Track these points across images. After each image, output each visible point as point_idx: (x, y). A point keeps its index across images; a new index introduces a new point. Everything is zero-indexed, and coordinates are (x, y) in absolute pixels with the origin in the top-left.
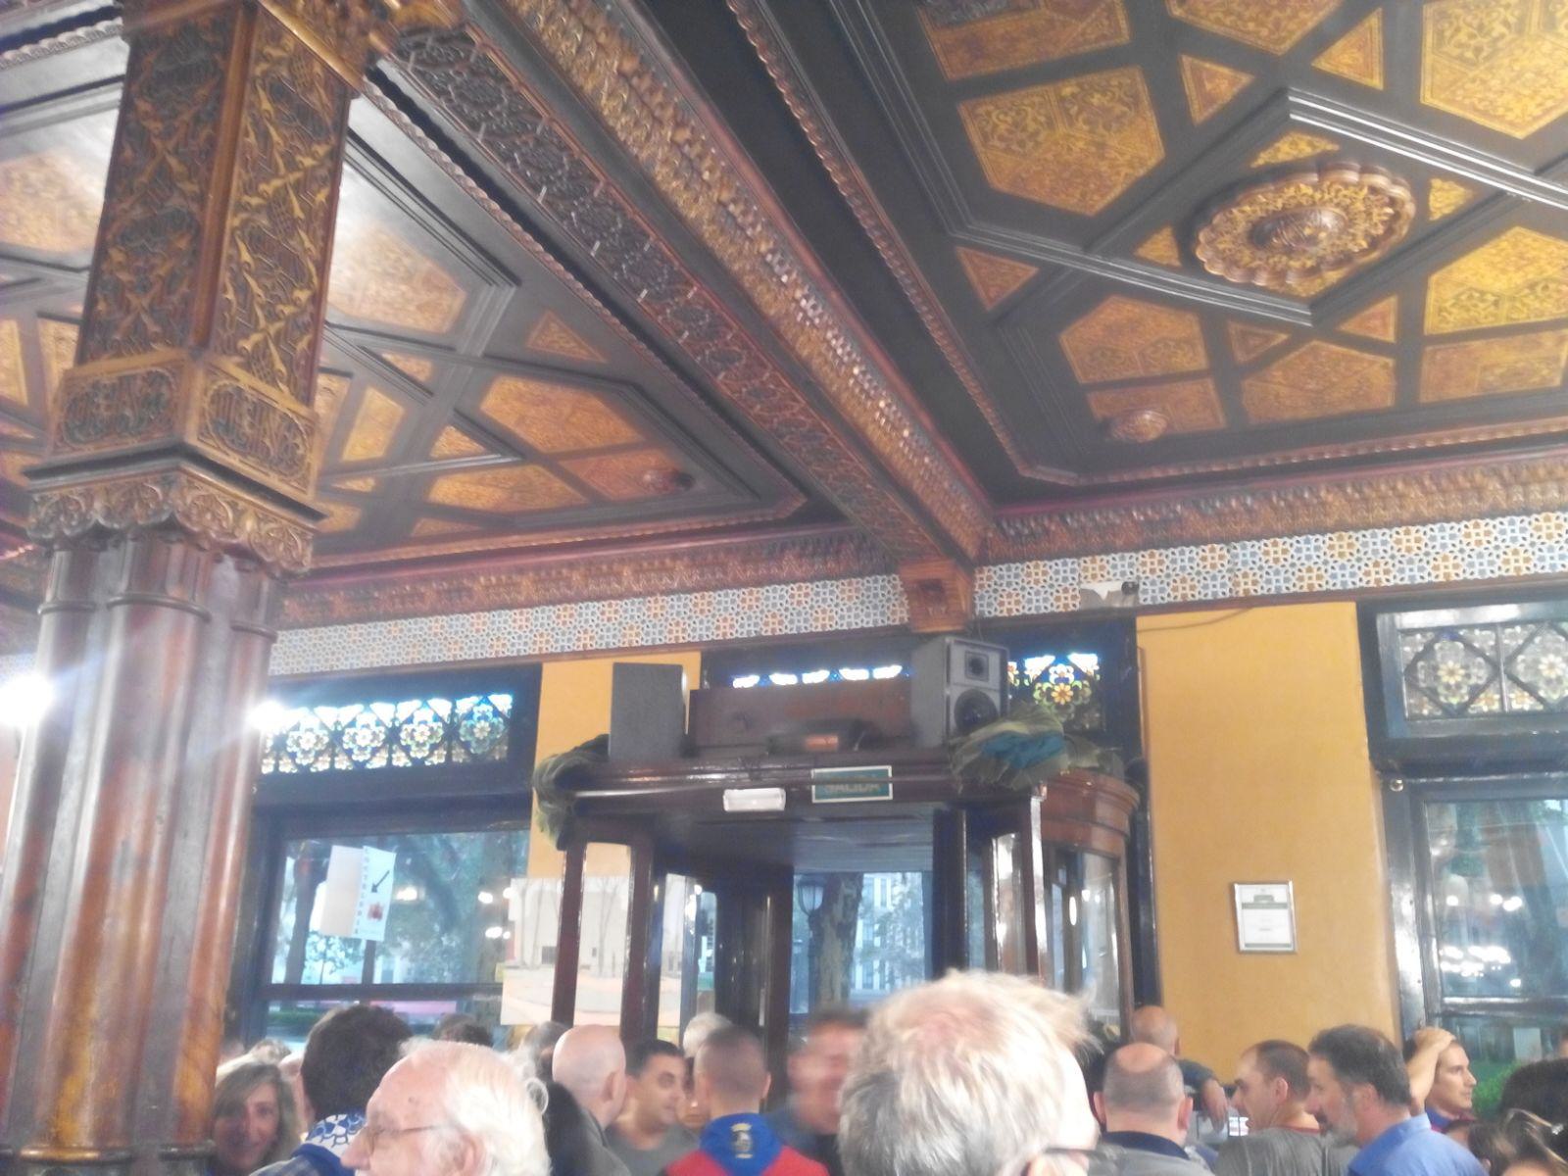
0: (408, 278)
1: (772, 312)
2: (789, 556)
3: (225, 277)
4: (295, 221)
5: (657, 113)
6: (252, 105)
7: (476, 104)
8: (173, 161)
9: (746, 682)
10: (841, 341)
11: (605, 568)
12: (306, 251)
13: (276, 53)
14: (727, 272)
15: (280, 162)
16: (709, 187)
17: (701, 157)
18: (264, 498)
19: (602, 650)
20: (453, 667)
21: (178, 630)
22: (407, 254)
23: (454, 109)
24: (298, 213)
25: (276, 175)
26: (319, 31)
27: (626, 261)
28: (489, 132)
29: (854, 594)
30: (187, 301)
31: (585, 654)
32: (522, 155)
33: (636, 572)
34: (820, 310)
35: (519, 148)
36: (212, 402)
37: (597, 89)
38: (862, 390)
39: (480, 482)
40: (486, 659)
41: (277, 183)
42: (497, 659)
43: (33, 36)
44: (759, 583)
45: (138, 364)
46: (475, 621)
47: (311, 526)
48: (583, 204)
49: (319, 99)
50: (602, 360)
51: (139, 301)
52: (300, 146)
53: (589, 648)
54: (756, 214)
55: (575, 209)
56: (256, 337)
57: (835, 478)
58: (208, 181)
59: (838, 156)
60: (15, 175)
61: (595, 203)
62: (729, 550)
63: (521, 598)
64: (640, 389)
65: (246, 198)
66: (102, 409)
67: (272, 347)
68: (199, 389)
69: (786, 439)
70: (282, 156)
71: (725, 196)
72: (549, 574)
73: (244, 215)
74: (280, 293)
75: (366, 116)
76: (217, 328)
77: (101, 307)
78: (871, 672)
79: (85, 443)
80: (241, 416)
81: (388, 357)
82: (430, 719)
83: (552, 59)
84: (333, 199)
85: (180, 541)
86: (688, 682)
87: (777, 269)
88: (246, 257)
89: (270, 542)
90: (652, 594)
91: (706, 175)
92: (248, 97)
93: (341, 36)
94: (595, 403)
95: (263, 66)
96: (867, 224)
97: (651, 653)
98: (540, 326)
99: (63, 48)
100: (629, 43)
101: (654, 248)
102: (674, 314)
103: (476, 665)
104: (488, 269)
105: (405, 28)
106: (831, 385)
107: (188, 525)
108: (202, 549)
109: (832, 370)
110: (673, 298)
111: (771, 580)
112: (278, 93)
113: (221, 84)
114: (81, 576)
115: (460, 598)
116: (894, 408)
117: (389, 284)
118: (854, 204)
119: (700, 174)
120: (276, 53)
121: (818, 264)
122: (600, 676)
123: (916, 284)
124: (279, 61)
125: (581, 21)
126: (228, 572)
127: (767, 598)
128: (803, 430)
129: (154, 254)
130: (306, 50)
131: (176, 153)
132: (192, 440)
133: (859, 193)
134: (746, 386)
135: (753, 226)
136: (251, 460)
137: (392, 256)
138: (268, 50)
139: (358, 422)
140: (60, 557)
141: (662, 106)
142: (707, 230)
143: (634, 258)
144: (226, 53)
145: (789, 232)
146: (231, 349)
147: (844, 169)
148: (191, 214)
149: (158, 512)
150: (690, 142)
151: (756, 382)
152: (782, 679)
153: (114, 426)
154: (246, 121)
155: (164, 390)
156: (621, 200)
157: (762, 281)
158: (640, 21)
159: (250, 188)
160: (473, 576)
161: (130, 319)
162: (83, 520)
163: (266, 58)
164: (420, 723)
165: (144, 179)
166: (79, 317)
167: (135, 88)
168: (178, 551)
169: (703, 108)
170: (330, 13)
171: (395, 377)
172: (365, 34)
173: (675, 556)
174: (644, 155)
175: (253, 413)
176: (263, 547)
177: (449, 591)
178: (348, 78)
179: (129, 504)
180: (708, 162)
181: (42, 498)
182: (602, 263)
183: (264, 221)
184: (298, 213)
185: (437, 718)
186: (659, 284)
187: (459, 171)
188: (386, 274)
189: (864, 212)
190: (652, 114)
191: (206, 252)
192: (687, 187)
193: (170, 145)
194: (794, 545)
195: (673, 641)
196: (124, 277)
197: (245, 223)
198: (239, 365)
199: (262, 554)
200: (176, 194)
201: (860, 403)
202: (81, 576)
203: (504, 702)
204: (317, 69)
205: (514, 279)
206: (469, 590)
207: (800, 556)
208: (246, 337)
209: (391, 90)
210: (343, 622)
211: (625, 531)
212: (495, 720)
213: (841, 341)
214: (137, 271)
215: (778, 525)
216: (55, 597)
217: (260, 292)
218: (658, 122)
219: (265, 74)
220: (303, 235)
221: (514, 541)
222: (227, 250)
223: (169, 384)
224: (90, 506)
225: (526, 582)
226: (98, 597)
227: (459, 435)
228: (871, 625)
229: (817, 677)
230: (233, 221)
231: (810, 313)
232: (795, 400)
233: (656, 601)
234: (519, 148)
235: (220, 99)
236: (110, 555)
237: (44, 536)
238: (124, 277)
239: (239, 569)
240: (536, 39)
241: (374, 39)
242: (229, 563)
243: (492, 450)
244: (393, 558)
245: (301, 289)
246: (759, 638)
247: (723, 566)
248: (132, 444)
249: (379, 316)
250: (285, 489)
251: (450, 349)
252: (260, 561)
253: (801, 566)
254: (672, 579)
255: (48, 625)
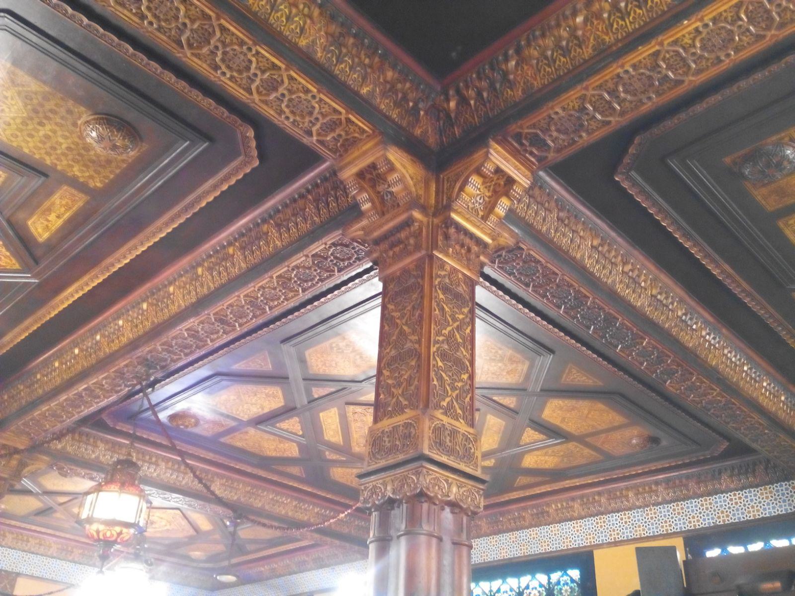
0: (502, 360)
1: (691, 345)
2: (724, 476)
3: (432, 374)
4: (458, 344)
5: (613, 260)
6: (436, 297)
7: (527, 276)
8: (405, 328)
9: (713, 553)
10: (733, 354)
11: (618, 493)
12: (464, 356)
13: (443, 273)
14: (662, 329)
15: (450, 319)
16: (646, 289)
17: (639, 276)
18: (459, 476)
19: (651, 537)
20: (584, 550)
21: (429, 546)
22: (500, 349)
23: (517, 280)
24: (460, 340)
25: (449, 325)
26: (459, 260)
27: (608, 333)
28: (533, 286)
29: (769, 495)
30: (417, 388)
31: (616, 544)
32: (551, 293)
33: (636, 494)
34: (718, 339)
35: (549, 291)
36: (433, 432)
37: (583, 256)
38: (751, 378)
39: (546, 454)
40: (562, 550)
41: (449, 329)
42: (485, 563)
43: (338, 287)
44: (710, 494)
45: (399, 420)
46: (553, 529)
47: (481, 487)
48: (583, 310)
49: (462, 289)
50: (600, 383)
51: (398, 391)
52: (457, 310)
53: (617, 540)
54: (672, 297)
55: (579, 312)
56: (448, 399)
57: (744, 429)
58: (421, 333)
59: (713, 261)
60: (334, 345)
61: (589, 308)
62: (688, 477)
63: (576, 515)
64: (623, 396)
65: (437, 338)
66: (387, 443)
67: (455, 403)
68: (427, 426)
69: (712, 411)
70: (450, 316)
71: (654, 292)
72: (588, 500)
73: (437, 346)
74: (455, 377)
75: (482, 294)
76: (431, 398)
77: (382, 396)
78: (790, 541)
79: (381, 459)
80: (445, 437)
81: (495, 398)
82: (537, 586)
83: (560, 248)
84: (473, 331)
85: (426, 501)
86: (680, 556)
87: (689, 322)
88: (440, 364)
89: (464, 498)
90: (647, 506)
91: (643, 284)
92: (434, 294)
93: (469, 260)
94: (600, 406)
95: (439, 280)
96: (737, 291)
97: (654, 540)
98: (567, 371)
99: (351, 289)
100: (595, 232)
101: (622, 324)
102: (637, 354)
103: (557, 554)
104: (541, 350)
105: (494, 250)
106: (733, 378)
107: (429, 493)
108: (435, 504)
109: (731, 370)
110: (635, 347)
111: (716, 492)
112: (446, 290)
113: (422, 291)
114: (384, 524)
115: (544, 517)
116: (772, 385)
117: (493, 364)
118: (727, 282)
119: (640, 284)
120: (443, 273)
121: (712, 316)
122: (628, 557)
123: (772, 316)
124: (444, 276)
125: (570, 229)
126: (447, 515)
127: (716, 502)
128: (721, 405)
129: (402, 369)
130: (455, 269)
131: (406, 324)
132: (426, 452)
133: (729, 276)
134: (683, 386)
135: (672, 303)
136: (452, 458)
137: (494, 351)
138: (439, 273)
139: (484, 432)
140: (375, 515)
141: (615, 257)
142: (648, 310)
143: (612, 331)
144: (423, 277)
145: (693, 303)
146: (438, 406)
147: (718, 266)
148: (415, 349)
149: (415, 488)
150: (632, 270)
151: (689, 383)
152: (735, 550)
153: (393, 450)
154: (434, 304)
155: (412, 430)
156: (602, 304)
157: (682, 330)
158: (599, 221)
159: (439, 333)
160: (548, 505)
161: (394, 400)
162: (384, 496)
163: (439, 276)
164: (533, 589)
165: (394, 338)
166: (373, 403)
167: (386, 300)
168: (425, 506)
169: (636, 253)
170: (463, 251)
171: (498, 407)
172: (478, 257)
173: (657, 483)
174: (610, 281)
175: (450, 435)
176: (461, 500)
177: (537, 514)
178: (473, 277)
179: (402, 486)
180: (643, 278)
181: (365, 487)
182: (596, 336)
183: (446, 347)
184: (460, 340)
185: (541, 585)
186: (627, 341)
187: (520, 306)
188: (492, 360)
189: (733, 285)
190: (610, 261)
191: (423, 366)
192: (634, 292)
193: (404, 321)
194: (726, 470)
195: (665, 532)
196: (390, 382)
197: (438, 349)
198: (442, 413)
199: (461, 504)
200: (408, 341)
201: (751, 386)
202: (384, 524)
203: (575, 574)
204: (460, 276)
205: (551, 351)
206: (548, 512)
207: (731, 476)
208: (444, 400)
209: (494, 282)
210: (487, 535)
211: (627, 472)
212: (572, 585)
213: (733, 354)
214: (395, 378)
215: (714, 459)
216: (374, 534)
217: (447, 378)
218: (614, 264)
219: (440, 283)
220: (463, 349)
221: (567, 483)
222: (432, 362)
223: (414, 427)
224: (386, 489)
225: (576, 505)
226: (393, 533)
227: (533, 432)
228: (784, 512)
229: (756, 547)
230: (433, 349)
231: (713, 342)
232: (713, 389)
233: (651, 510)
234: (549, 291)
235: (422, 297)
236: (396, 512)
237: (367, 505)
238: (390, 382)
239: (452, 512)
240: (551, 241)
241: (482, 258)
242: (448, 509)
243: (550, 437)
244: (507, 499)
245: (464, 374)
246: (716, 526)
247: (686, 486)
248: (401, 457)
249: (490, 380)
250: (468, 470)
251: (525, 390)
252: (461, 507)
253: (733, 482)
254: (658, 496)
255: (372, 548)
